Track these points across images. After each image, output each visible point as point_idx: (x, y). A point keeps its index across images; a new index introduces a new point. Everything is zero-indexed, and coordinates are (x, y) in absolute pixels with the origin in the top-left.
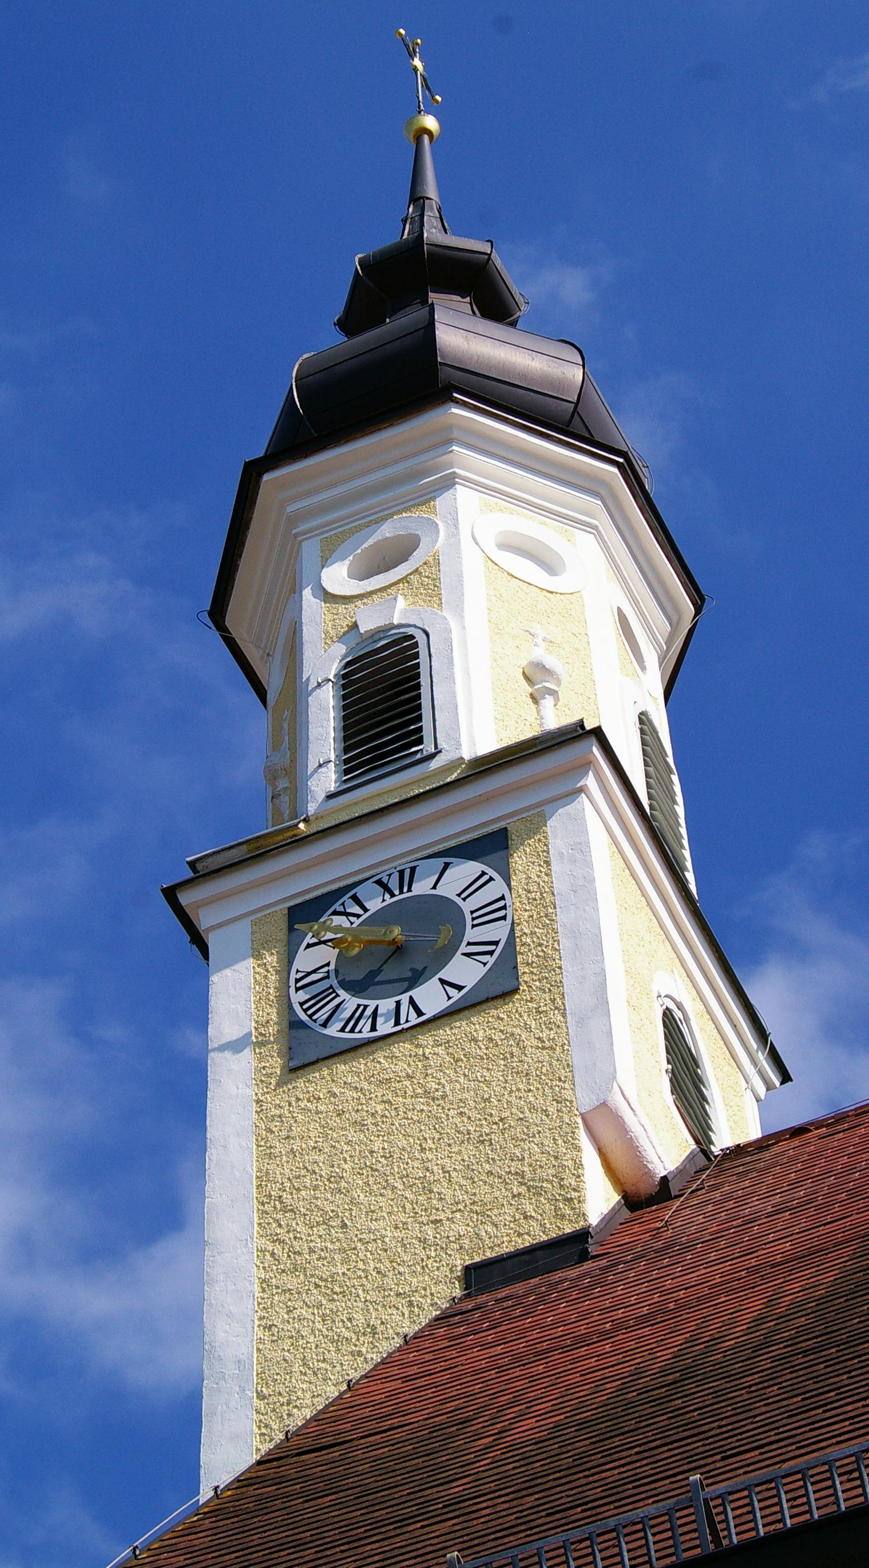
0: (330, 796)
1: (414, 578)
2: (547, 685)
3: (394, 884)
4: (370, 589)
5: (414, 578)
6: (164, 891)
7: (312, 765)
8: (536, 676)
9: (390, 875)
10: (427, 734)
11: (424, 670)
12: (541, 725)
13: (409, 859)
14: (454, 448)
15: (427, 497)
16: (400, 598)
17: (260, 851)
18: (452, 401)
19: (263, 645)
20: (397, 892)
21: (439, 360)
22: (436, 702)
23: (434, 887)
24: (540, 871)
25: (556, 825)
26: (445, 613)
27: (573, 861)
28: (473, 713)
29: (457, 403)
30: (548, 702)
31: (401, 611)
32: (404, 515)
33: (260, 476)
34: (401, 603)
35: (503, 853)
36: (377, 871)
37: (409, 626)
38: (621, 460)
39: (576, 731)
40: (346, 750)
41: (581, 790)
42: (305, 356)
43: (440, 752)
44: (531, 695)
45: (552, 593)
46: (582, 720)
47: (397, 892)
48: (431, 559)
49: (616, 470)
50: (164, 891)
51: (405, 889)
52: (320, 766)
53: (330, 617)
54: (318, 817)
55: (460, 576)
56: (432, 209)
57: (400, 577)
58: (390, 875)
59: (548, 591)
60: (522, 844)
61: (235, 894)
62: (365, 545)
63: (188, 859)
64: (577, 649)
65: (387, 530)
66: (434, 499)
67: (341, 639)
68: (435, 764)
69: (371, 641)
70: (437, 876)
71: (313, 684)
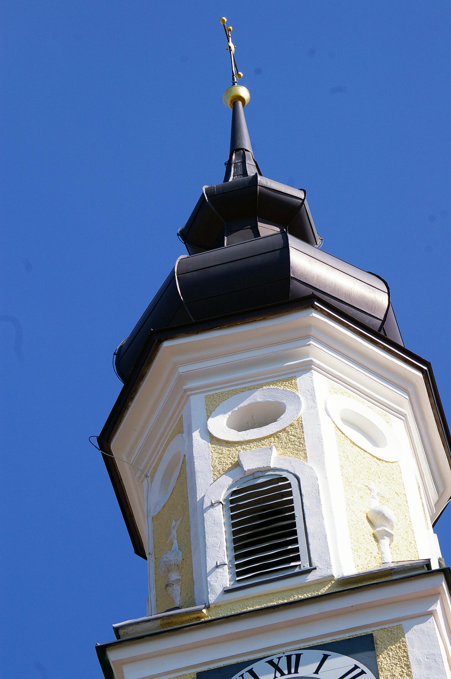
0: (227, 591)
1: (283, 435)
2: (387, 529)
3: (283, 665)
4: (247, 438)
5: (283, 435)
6: (98, 648)
7: (210, 565)
8: (377, 521)
9: (279, 658)
10: (303, 553)
11: (297, 505)
12: (382, 558)
13: (298, 646)
14: (311, 342)
15: (290, 376)
16: (274, 448)
17: (172, 626)
18: (313, 307)
19: (142, 468)
20: (286, 672)
21: (291, 275)
22: (308, 531)
23: (317, 672)
24: (402, 671)
25: (413, 637)
26: (310, 463)
27: (429, 668)
28: (337, 544)
29: (316, 309)
30: (385, 542)
31: (276, 459)
32: (271, 387)
33: (161, 342)
34: (275, 453)
35: (370, 653)
36: (269, 653)
37: (283, 470)
38: (425, 368)
39: (423, 568)
40: (237, 557)
41: (431, 614)
42: (181, 257)
43: (315, 569)
44: (373, 534)
45: (380, 460)
46: (429, 560)
47: (286, 672)
48: (296, 423)
49: (421, 375)
50: (98, 648)
51: (293, 670)
52: (217, 567)
53: (216, 455)
54: (217, 606)
55: (320, 439)
56: (250, 159)
57: (271, 433)
58: (279, 658)
59: (377, 459)
60: (387, 649)
61: (156, 656)
62: (242, 405)
63: (114, 625)
64: (400, 505)
65: (258, 396)
66: (295, 378)
67: (227, 472)
68: (311, 577)
69: (252, 477)
70: (318, 664)
71: (207, 504)
